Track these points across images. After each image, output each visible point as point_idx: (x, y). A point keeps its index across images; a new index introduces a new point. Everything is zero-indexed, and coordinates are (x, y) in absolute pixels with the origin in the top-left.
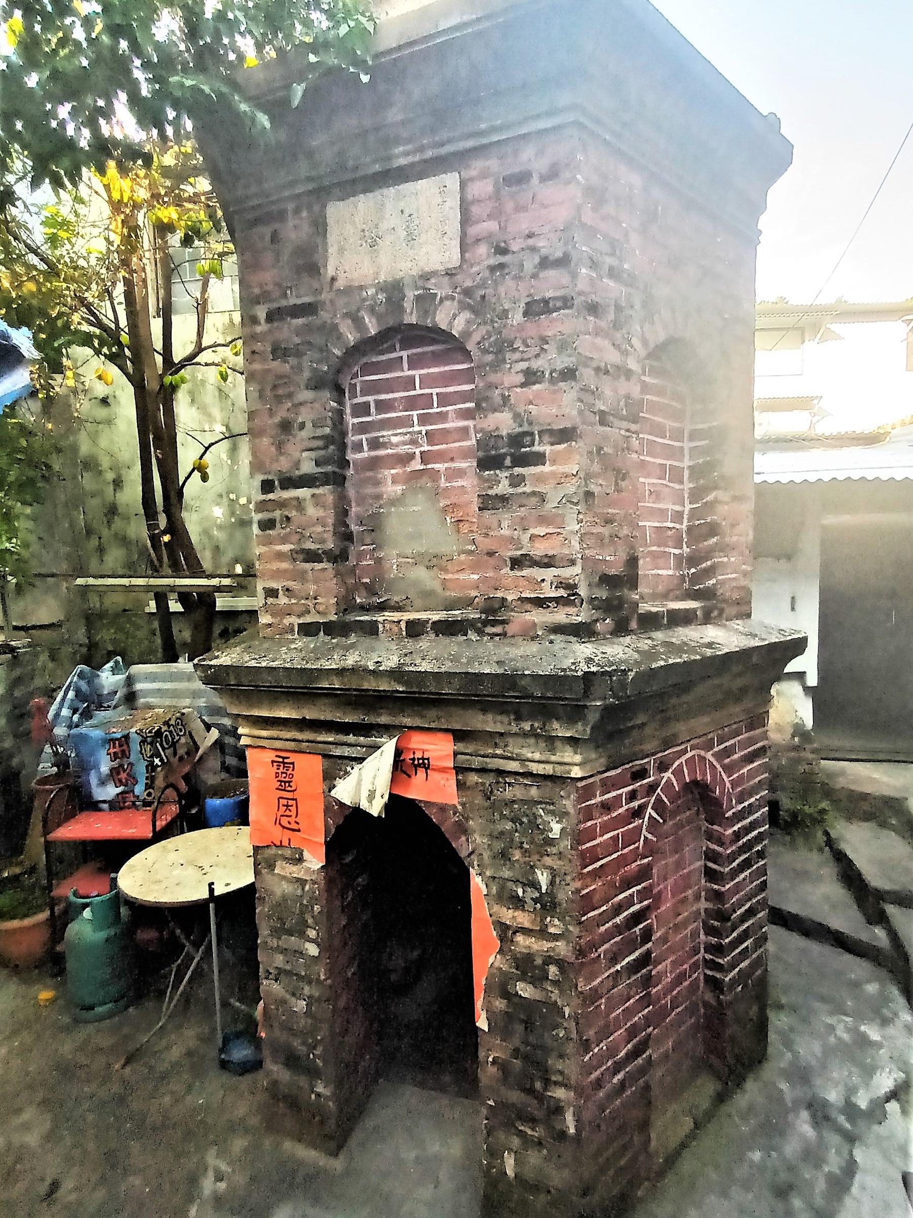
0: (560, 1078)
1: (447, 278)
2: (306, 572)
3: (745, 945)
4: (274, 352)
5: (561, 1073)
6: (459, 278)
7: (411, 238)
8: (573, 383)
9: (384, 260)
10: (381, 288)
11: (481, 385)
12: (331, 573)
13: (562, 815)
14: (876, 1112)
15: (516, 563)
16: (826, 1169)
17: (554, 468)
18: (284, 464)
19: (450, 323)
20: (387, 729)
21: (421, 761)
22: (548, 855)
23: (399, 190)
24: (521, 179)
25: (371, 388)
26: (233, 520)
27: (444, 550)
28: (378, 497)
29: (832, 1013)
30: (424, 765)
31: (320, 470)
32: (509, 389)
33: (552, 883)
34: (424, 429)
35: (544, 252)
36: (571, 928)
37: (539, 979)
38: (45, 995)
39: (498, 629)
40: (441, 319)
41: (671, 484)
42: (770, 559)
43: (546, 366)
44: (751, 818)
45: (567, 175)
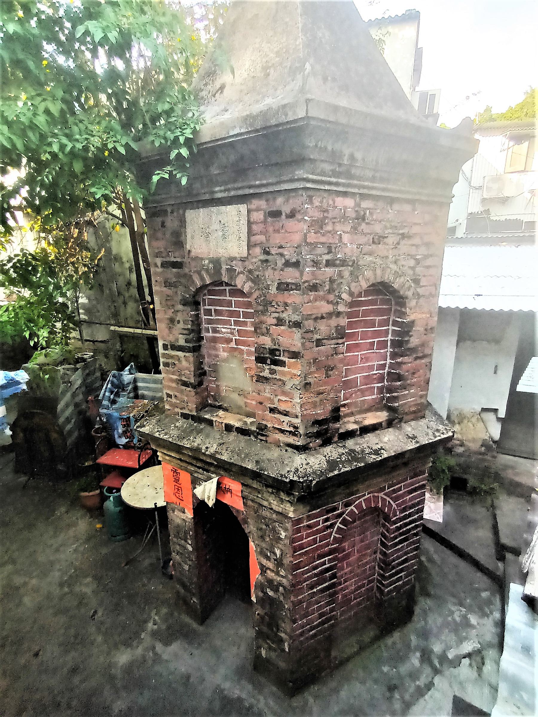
1: (241, 262)
3: (401, 575)
6: (246, 263)
7: (224, 237)
8: (299, 330)
10: (211, 261)
11: (257, 320)
12: (193, 393)
13: (286, 530)
14: (456, 663)
15: (272, 410)
16: (418, 683)
18: (171, 338)
19: (243, 287)
23: (219, 210)
24: (276, 214)
25: (212, 303)
27: (246, 388)
28: (217, 356)
29: (455, 604)
30: (229, 490)
31: (186, 344)
34: (237, 328)
35: (287, 257)
37: (276, 590)
38: (99, 526)
39: (264, 438)
41: (378, 351)
42: (484, 342)
44: (410, 519)
45: (298, 216)
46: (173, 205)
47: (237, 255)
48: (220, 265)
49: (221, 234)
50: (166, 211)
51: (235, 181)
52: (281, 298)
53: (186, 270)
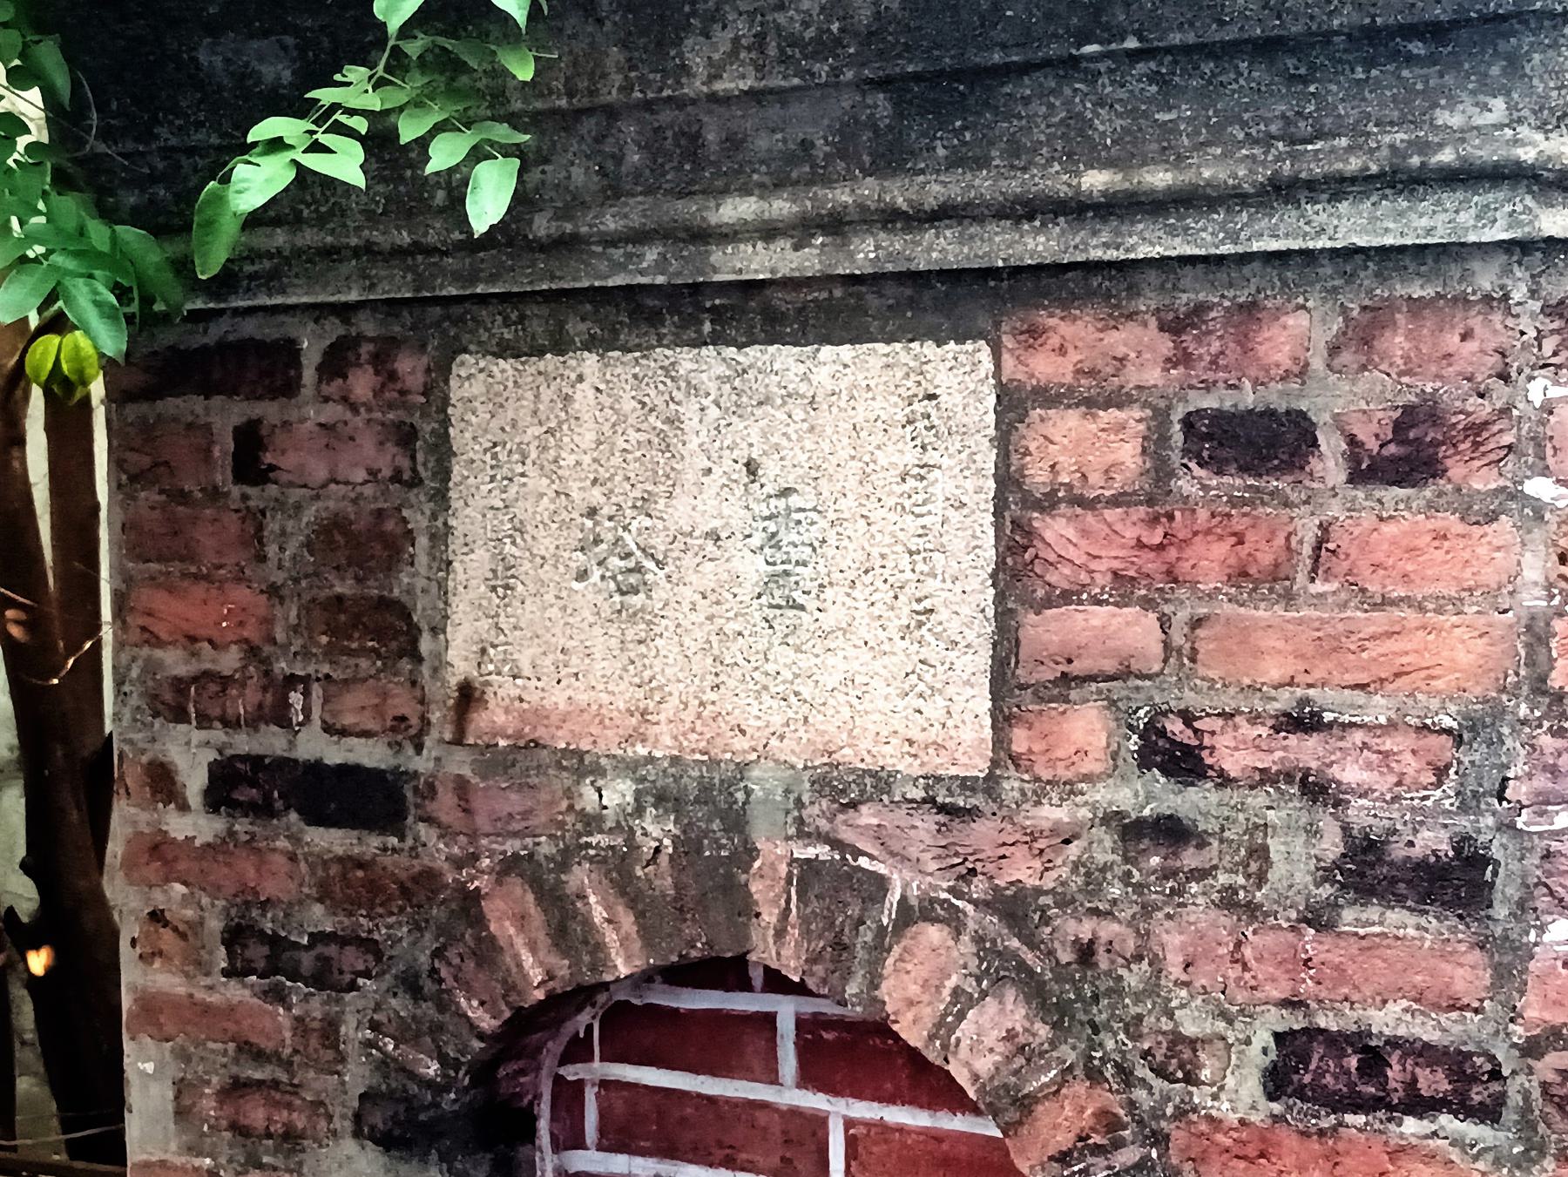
1: (926, 823)
4: (235, 936)
6: (982, 834)
7: (782, 594)
9: (675, 663)
10: (662, 796)
19: (943, 1029)
24: (1265, 444)
35: (1359, 813)
46: (344, 311)
47: (892, 757)
48: (737, 821)
49: (753, 568)
50: (289, 351)
51: (891, 158)
53: (438, 851)
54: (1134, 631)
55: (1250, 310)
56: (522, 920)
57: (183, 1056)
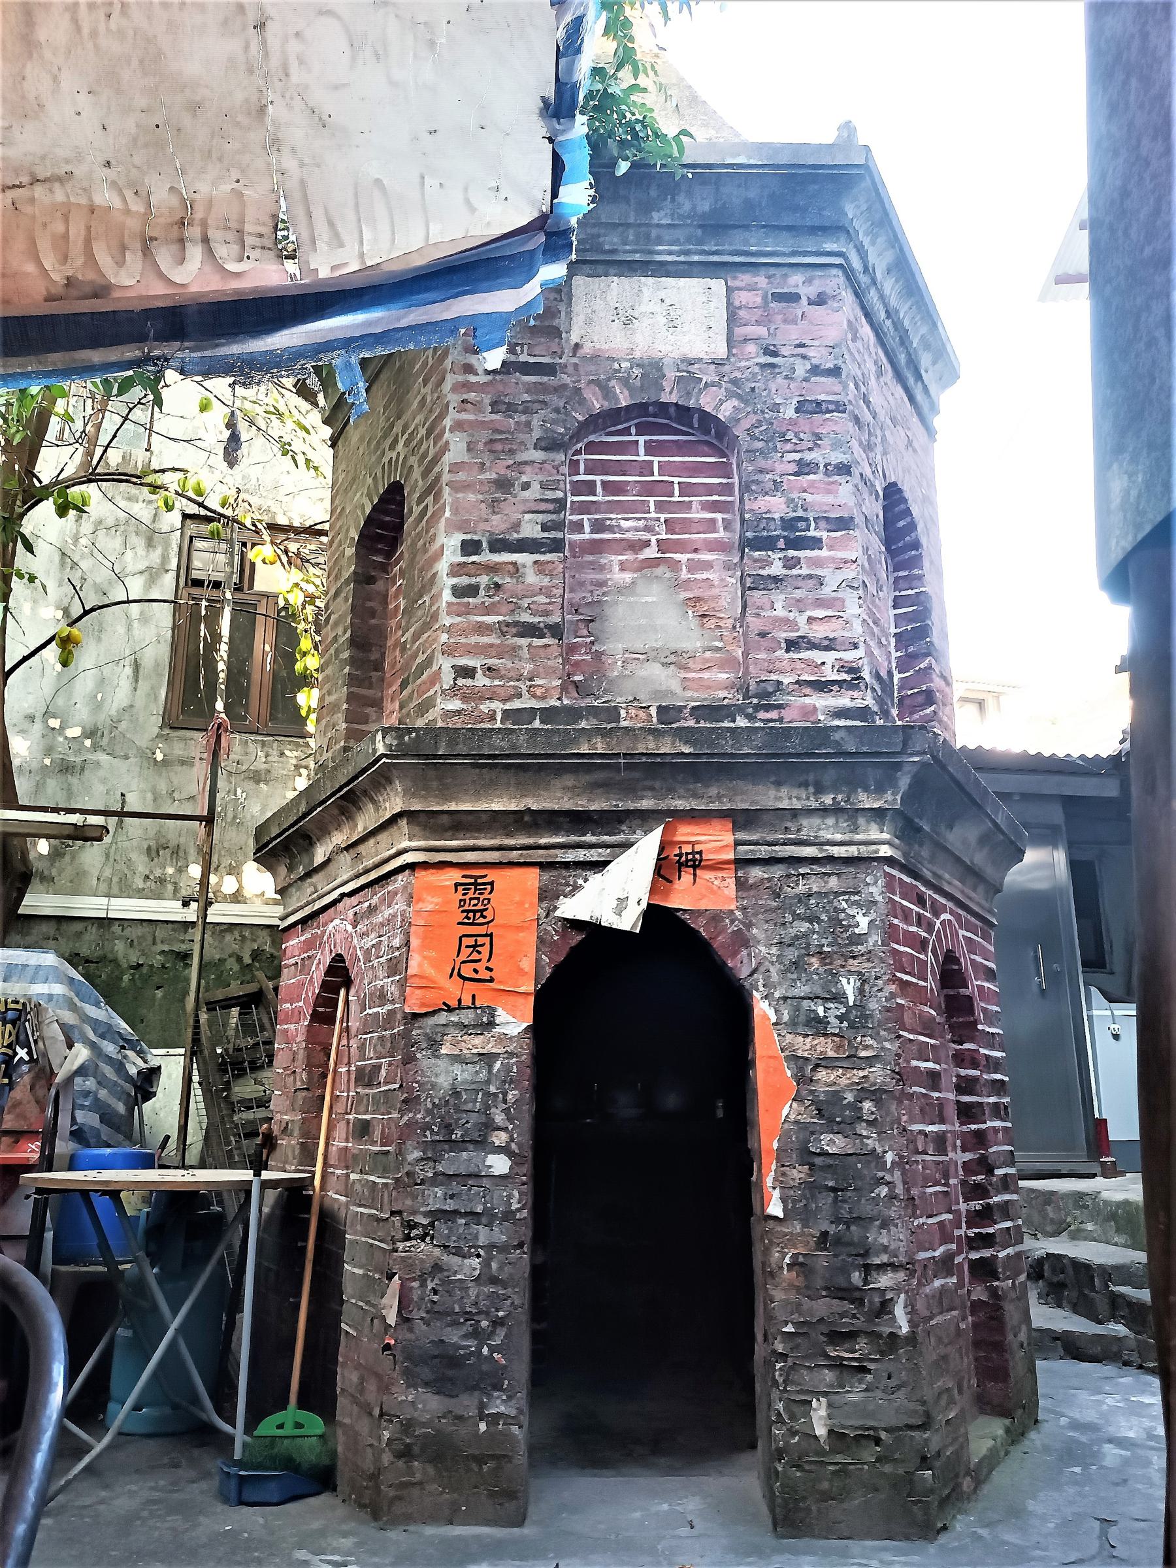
0: (885, 1258)
2: (520, 647)
4: (493, 404)
5: (885, 1249)
6: (727, 369)
8: (849, 478)
15: (792, 645)
17: (832, 553)
18: (498, 524)
20: (645, 819)
21: (690, 857)
22: (854, 958)
26: (47, 762)
27: (685, 645)
30: (695, 863)
31: (546, 535)
32: (781, 475)
33: (861, 991)
34: (663, 517)
35: (814, 361)
36: (887, 1045)
40: (707, 402)
43: (820, 459)
48: (660, 369)
52: (805, 424)
53: (566, 379)
54: (762, 331)
55: (785, 275)
56: (594, 394)
57: (469, 435)
